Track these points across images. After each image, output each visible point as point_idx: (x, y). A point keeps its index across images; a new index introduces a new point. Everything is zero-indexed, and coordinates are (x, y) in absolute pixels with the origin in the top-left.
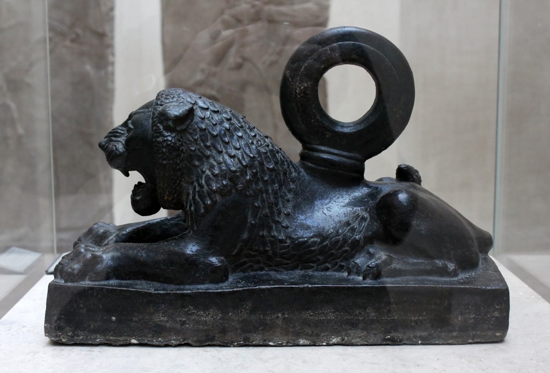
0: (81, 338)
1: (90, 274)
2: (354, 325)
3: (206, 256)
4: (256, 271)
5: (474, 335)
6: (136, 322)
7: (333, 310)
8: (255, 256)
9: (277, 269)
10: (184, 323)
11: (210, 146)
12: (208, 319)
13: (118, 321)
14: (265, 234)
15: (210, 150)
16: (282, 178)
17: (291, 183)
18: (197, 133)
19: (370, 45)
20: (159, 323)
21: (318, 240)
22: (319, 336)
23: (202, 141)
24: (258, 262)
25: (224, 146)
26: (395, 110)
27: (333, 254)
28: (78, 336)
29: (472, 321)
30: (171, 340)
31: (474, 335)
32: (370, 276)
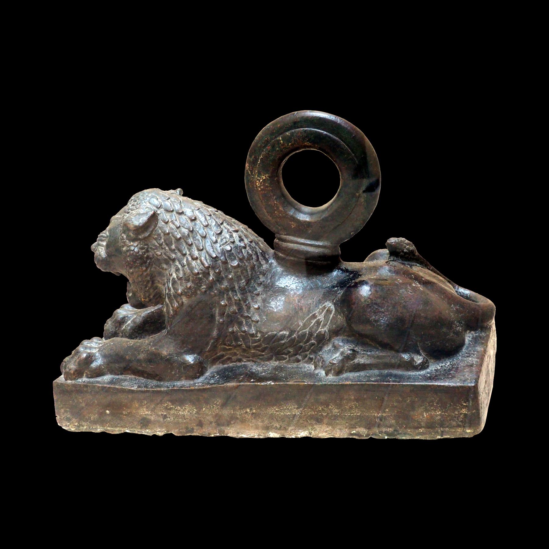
0: (85, 427)
1: (86, 371)
3: (179, 354)
4: (235, 362)
5: (442, 432)
6: (125, 415)
7: (296, 406)
8: (230, 349)
9: (254, 360)
10: (165, 417)
11: (174, 250)
12: (186, 413)
13: (112, 414)
14: (235, 330)
15: (175, 253)
16: (250, 273)
17: (261, 276)
18: (161, 238)
19: (323, 130)
20: (145, 416)
21: (287, 333)
22: (287, 430)
23: (167, 245)
24: (235, 354)
25: (188, 248)
26: (358, 194)
27: (301, 347)
28: (83, 426)
29: (439, 417)
30: (156, 432)
31: (442, 432)
32: (332, 372)
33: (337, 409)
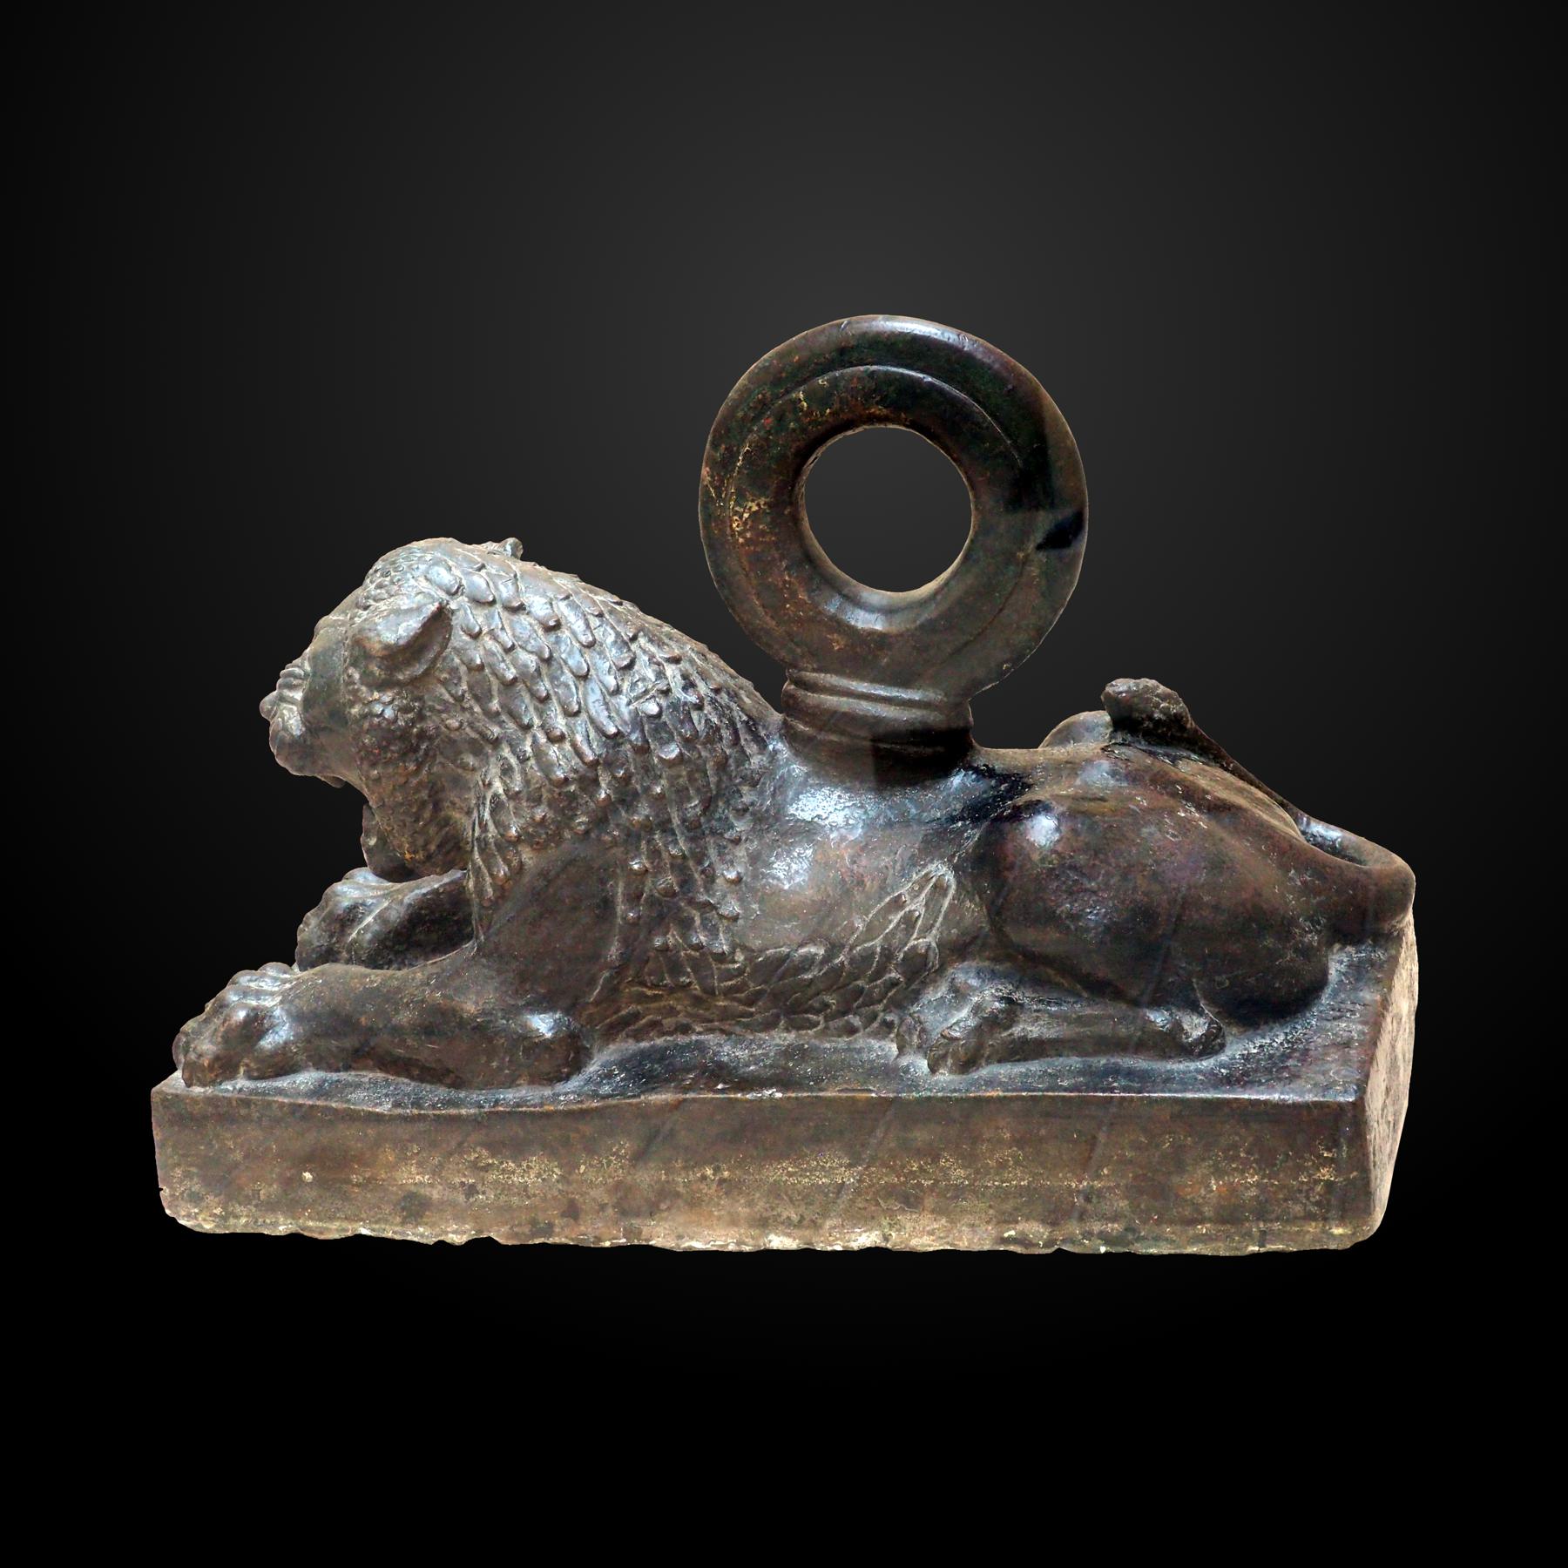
0: (243, 1220)
1: (246, 1061)
3: (513, 1012)
4: (670, 1034)
5: (1263, 1233)
6: (358, 1185)
7: (846, 1161)
8: (656, 998)
9: (726, 1027)
10: (471, 1190)
11: (498, 714)
12: (531, 1179)
13: (319, 1182)
14: (671, 941)
15: (501, 724)
16: (713, 780)
17: (745, 789)
18: (460, 679)
19: (922, 371)
20: (413, 1189)
21: (818, 951)
22: (821, 1227)
23: (477, 698)
24: (672, 1012)
25: (536, 709)
26: (1021, 555)
27: (860, 991)
28: (237, 1217)
29: (1253, 1192)
30: (447, 1233)
31: (1263, 1233)
32: (950, 1061)
33: (964, 1167)
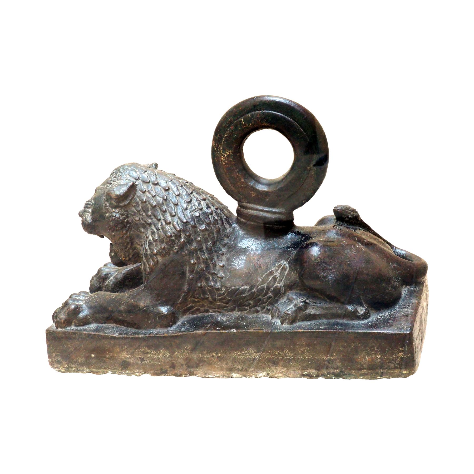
1: (74, 321)
2: (275, 363)
3: (155, 306)
4: (203, 312)
5: (382, 373)
6: (108, 358)
7: (256, 351)
8: (198, 302)
9: (220, 311)
10: (142, 360)
11: (150, 216)
12: (160, 356)
13: (96, 357)
14: (203, 285)
15: (151, 219)
16: (216, 236)
17: (225, 239)
18: (139, 205)
19: (279, 112)
20: (125, 359)
22: (248, 371)
23: (144, 211)
24: (203, 306)
25: (162, 214)
26: (309, 168)
27: (260, 300)
28: (72, 368)
29: (379, 360)
31: (382, 373)
32: (287, 321)
33: (291, 353)
